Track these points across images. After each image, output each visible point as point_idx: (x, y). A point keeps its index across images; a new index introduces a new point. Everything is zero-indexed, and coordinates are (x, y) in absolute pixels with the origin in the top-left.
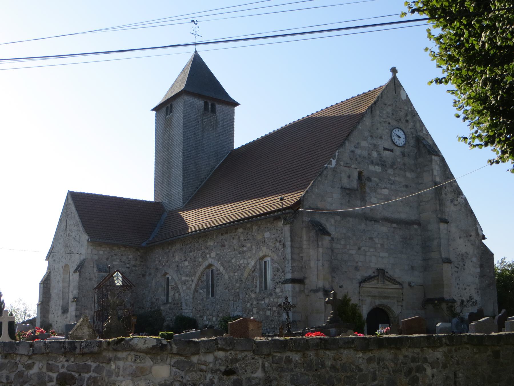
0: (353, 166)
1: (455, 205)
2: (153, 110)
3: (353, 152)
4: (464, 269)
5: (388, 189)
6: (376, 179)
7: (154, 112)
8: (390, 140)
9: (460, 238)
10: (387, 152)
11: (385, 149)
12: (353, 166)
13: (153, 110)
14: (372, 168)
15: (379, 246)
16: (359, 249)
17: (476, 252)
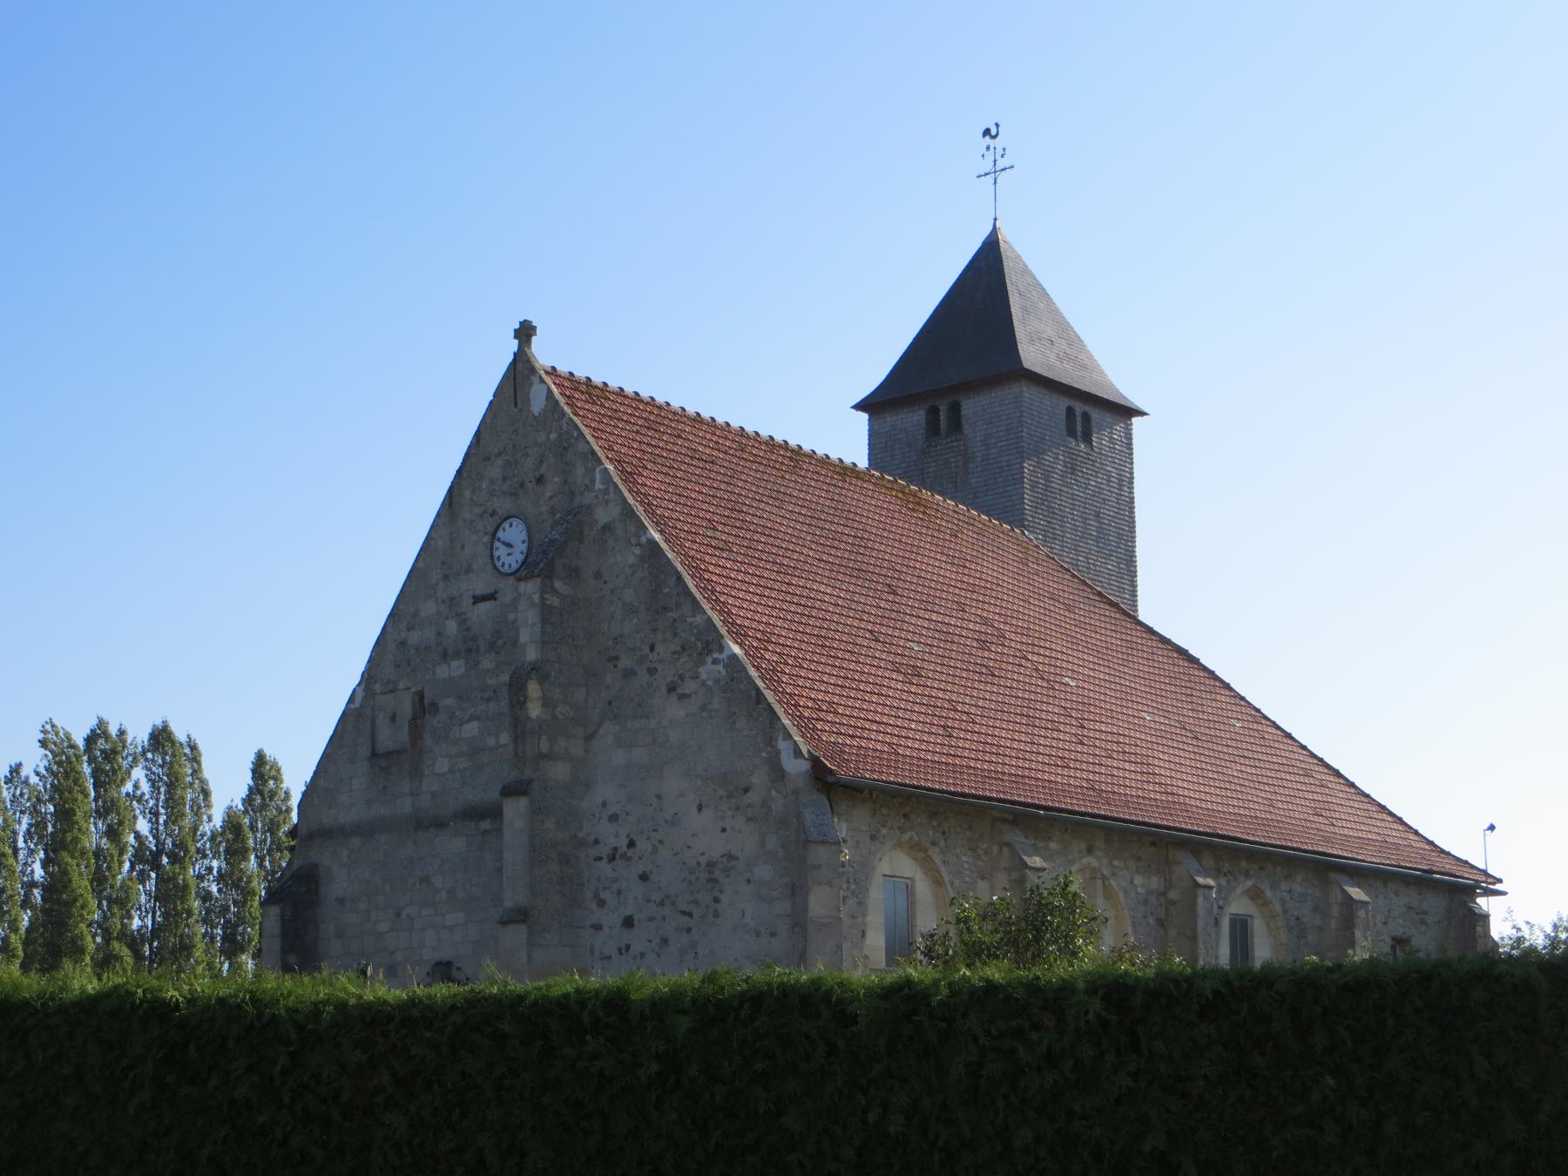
0: (401, 686)
1: (682, 697)
2: (860, 407)
3: (403, 644)
4: (716, 914)
5: (478, 718)
6: (449, 701)
7: (865, 416)
8: (489, 567)
9: (700, 808)
10: (484, 607)
11: (478, 599)
12: (401, 686)
13: (860, 407)
14: (442, 671)
15: (444, 895)
16: (398, 915)
17: (772, 843)
